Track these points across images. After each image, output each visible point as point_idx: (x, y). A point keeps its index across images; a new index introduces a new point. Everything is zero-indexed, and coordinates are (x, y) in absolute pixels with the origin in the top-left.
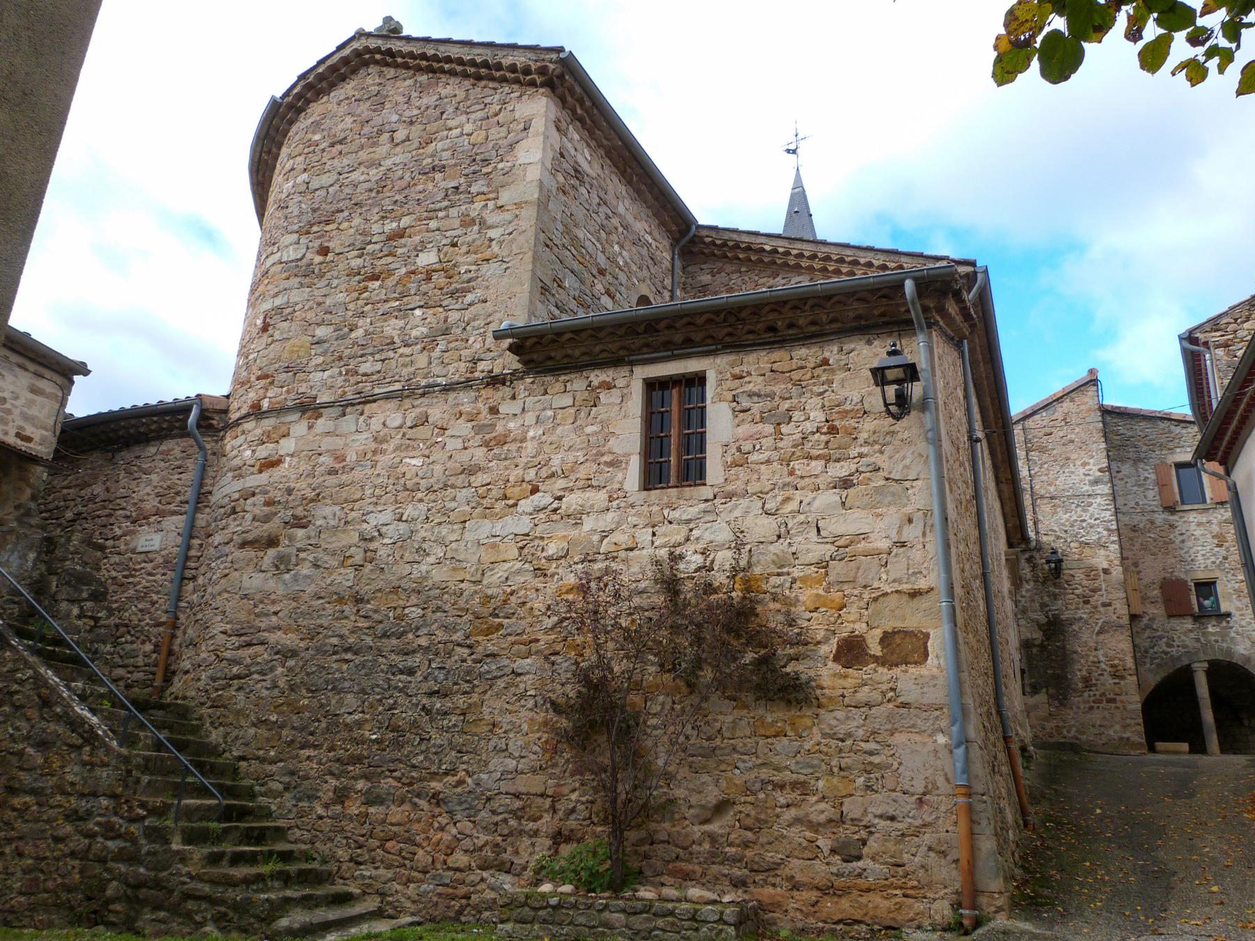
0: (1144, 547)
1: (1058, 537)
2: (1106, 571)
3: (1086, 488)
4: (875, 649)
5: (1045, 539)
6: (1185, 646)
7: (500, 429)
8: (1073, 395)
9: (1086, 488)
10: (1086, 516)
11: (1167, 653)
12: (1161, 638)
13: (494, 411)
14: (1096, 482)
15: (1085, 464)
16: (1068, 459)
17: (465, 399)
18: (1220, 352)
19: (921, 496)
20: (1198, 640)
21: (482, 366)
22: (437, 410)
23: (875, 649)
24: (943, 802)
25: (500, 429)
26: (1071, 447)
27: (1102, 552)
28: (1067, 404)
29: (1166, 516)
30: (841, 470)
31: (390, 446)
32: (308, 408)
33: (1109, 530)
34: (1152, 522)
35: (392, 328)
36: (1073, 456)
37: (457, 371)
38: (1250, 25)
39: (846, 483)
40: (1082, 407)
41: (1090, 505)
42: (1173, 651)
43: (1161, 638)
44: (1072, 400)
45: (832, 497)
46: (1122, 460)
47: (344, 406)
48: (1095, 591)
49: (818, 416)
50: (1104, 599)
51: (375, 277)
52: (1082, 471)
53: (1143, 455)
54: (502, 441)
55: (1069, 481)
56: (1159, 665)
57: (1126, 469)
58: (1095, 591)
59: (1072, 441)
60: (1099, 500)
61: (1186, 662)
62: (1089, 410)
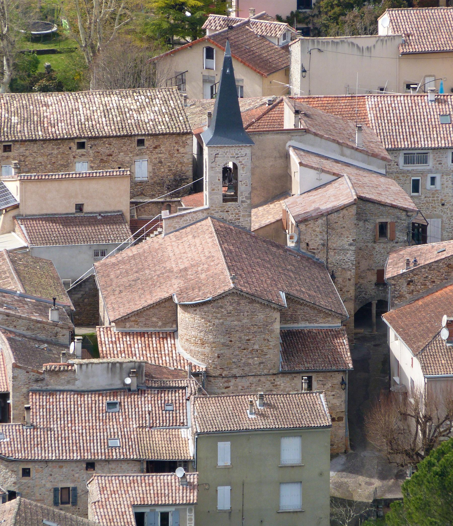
0: (363, 257)
1: (335, 265)
2: (349, 280)
3: (347, 247)
4: (336, 419)
5: (330, 265)
6: (371, 295)
7: (276, 383)
8: (348, 208)
9: (347, 247)
10: (345, 258)
11: (364, 297)
12: (363, 291)
13: (274, 380)
14: (351, 245)
15: (347, 237)
16: (342, 234)
17: (269, 378)
18: (393, 286)
19: (343, 399)
20: (375, 293)
21: (271, 371)
22: (263, 379)
23: (336, 419)
24: (344, 438)
25: (276, 383)
26: (344, 229)
27: (349, 272)
28: (345, 211)
29: (372, 244)
30: (333, 393)
31: (254, 385)
32: (235, 377)
33: (352, 264)
34: (367, 246)
35: (250, 361)
36: (344, 233)
37: (266, 372)
38: (423, 279)
39: (334, 395)
40: (350, 213)
41: (347, 253)
42: (366, 297)
43: (363, 291)
44: (347, 210)
45: (332, 397)
46: (360, 220)
47: (242, 377)
48: (345, 286)
49: (330, 385)
50: (347, 290)
51: (244, 349)
52: (346, 239)
53: (368, 218)
54: (276, 385)
55: (341, 243)
56: (361, 302)
57: (361, 223)
58: (345, 286)
59: (344, 227)
60: (350, 252)
61: (370, 301)
62: (352, 215)
